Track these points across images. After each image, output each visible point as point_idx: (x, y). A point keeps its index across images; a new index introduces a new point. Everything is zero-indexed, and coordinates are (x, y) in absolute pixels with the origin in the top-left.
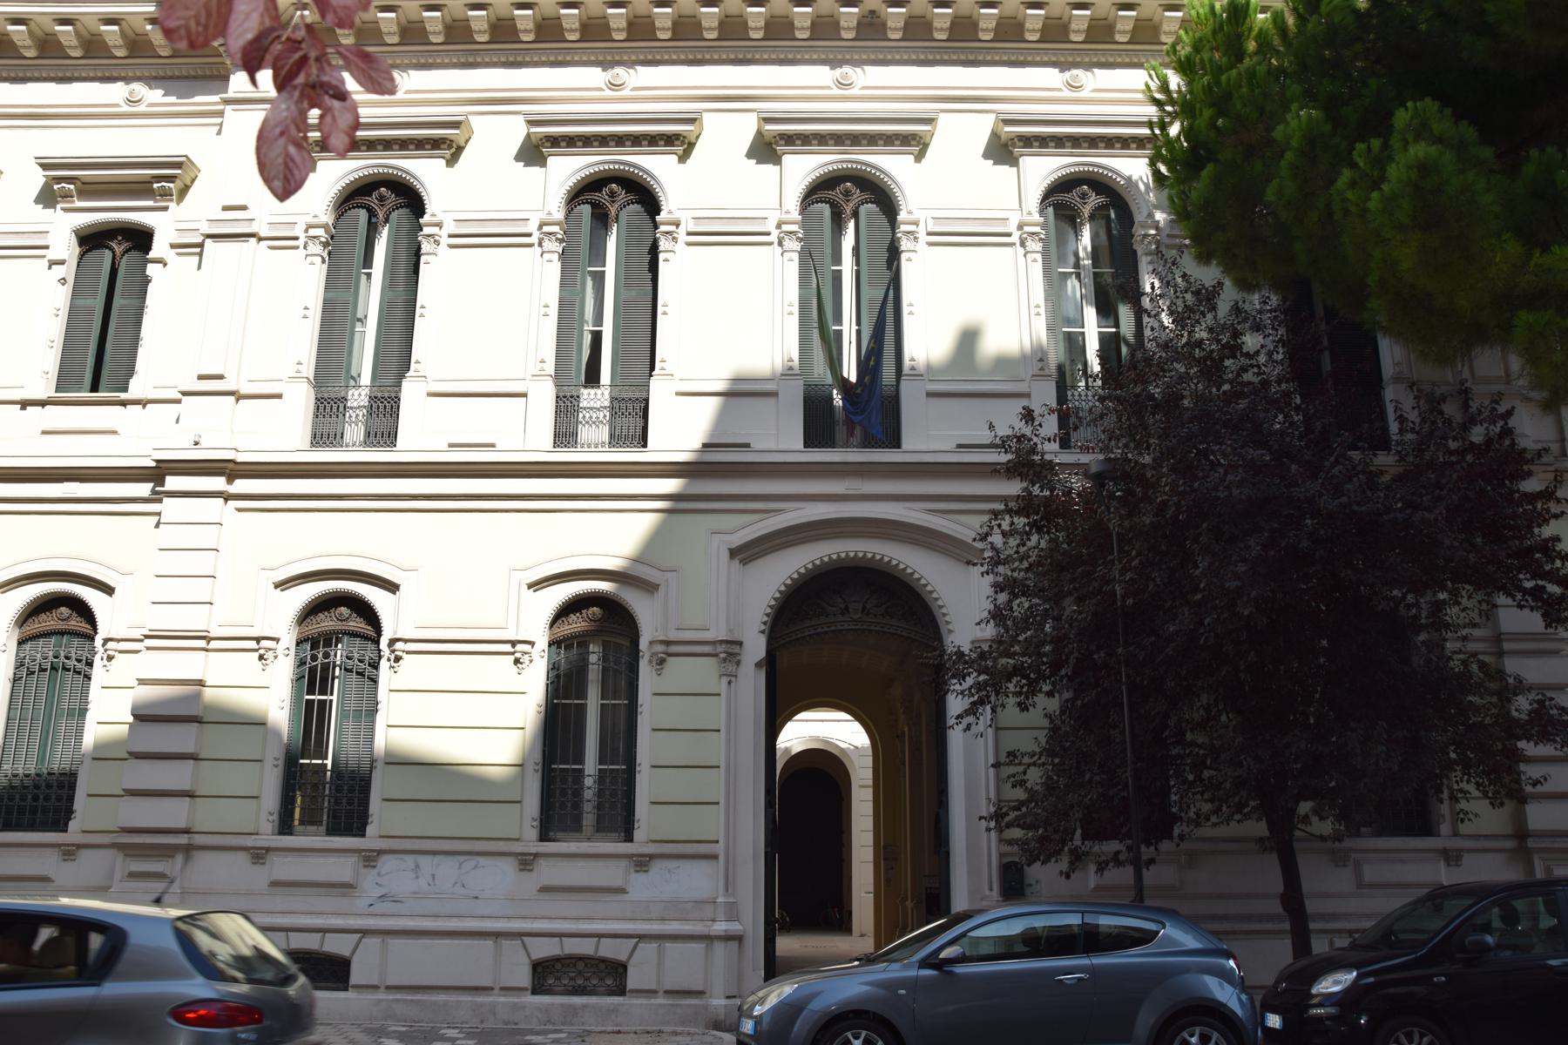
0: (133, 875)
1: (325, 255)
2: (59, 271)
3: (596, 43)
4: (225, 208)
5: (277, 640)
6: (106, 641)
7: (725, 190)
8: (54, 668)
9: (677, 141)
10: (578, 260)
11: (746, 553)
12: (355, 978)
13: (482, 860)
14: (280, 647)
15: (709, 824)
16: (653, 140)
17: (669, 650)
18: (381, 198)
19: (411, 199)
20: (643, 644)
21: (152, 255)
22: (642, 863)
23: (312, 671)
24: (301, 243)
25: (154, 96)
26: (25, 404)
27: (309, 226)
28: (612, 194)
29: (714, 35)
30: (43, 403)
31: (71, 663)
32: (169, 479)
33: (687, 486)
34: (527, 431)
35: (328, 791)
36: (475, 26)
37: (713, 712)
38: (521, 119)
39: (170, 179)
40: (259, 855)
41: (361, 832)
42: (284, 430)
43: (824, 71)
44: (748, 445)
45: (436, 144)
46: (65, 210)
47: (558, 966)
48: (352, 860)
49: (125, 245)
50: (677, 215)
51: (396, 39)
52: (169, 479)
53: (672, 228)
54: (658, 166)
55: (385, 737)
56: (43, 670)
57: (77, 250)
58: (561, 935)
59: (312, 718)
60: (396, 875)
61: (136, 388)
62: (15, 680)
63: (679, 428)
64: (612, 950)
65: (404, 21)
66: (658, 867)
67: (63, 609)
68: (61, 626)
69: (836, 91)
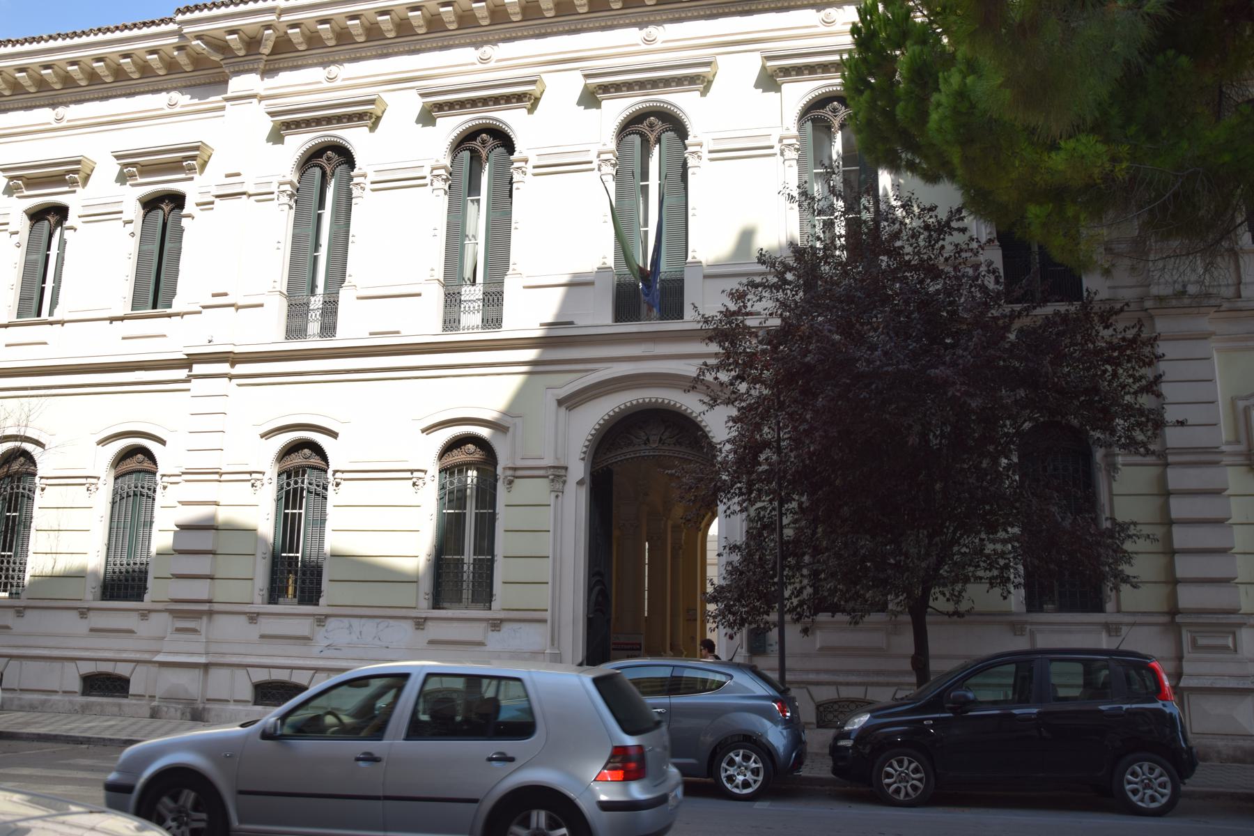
0: (179, 630)
1: (292, 203)
2: (130, 228)
3: (469, 29)
4: (228, 176)
5: (425, 472)
6: (335, 472)
7: (563, 133)
8: (135, 495)
9: (697, 80)
10: (629, 179)
11: (570, 402)
12: (133, 689)
13: (392, 622)
14: (428, 477)
15: (541, 598)
16: (679, 81)
17: (516, 473)
18: (329, 159)
19: (676, 125)
20: (499, 470)
21: (185, 212)
22: (496, 624)
23: (288, 493)
24: (427, 181)
25: (182, 100)
26: (112, 320)
27: (281, 184)
28: (483, 142)
29: (552, 14)
30: (122, 319)
31: (313, 488)
32: (195, 366)
33: (541, 354)
34: (423, 320)
35: (295, 573)
36: (384, 27)
37: (545, 518)
38: (579, 74)
39: (193, 158)
40: (253, 617)
41: (139, 598)
42: (266, 329)
43: (634, 31)
44: (571, 323)
45: (520, 97)
46: (132, 185)
47: (836, 707)
48: (310, 620)
49: (171, 205)
50: (525, 154)
51: (332, 43)
52: (195, 366)
53: (522, 164)
54: (683, 102)
55: (333, 541)
56: (128, 496)
57: (142, 212)
58: (836, 684)
59: (289, 527)
60: (337, 631)
61: (178, 305)
62: (114, 503)
63: (529, 310)
64: (122, 670)
65: (397, 20)
66: (506, 627)
67: (139, 456)
68: (139, 467)
69: (644, 47)
